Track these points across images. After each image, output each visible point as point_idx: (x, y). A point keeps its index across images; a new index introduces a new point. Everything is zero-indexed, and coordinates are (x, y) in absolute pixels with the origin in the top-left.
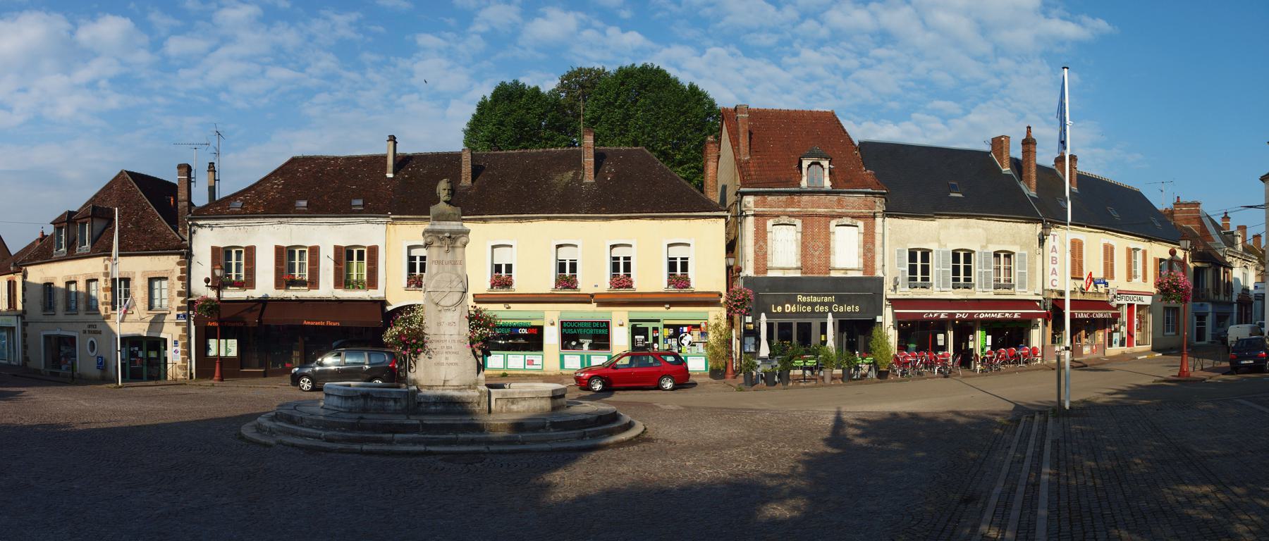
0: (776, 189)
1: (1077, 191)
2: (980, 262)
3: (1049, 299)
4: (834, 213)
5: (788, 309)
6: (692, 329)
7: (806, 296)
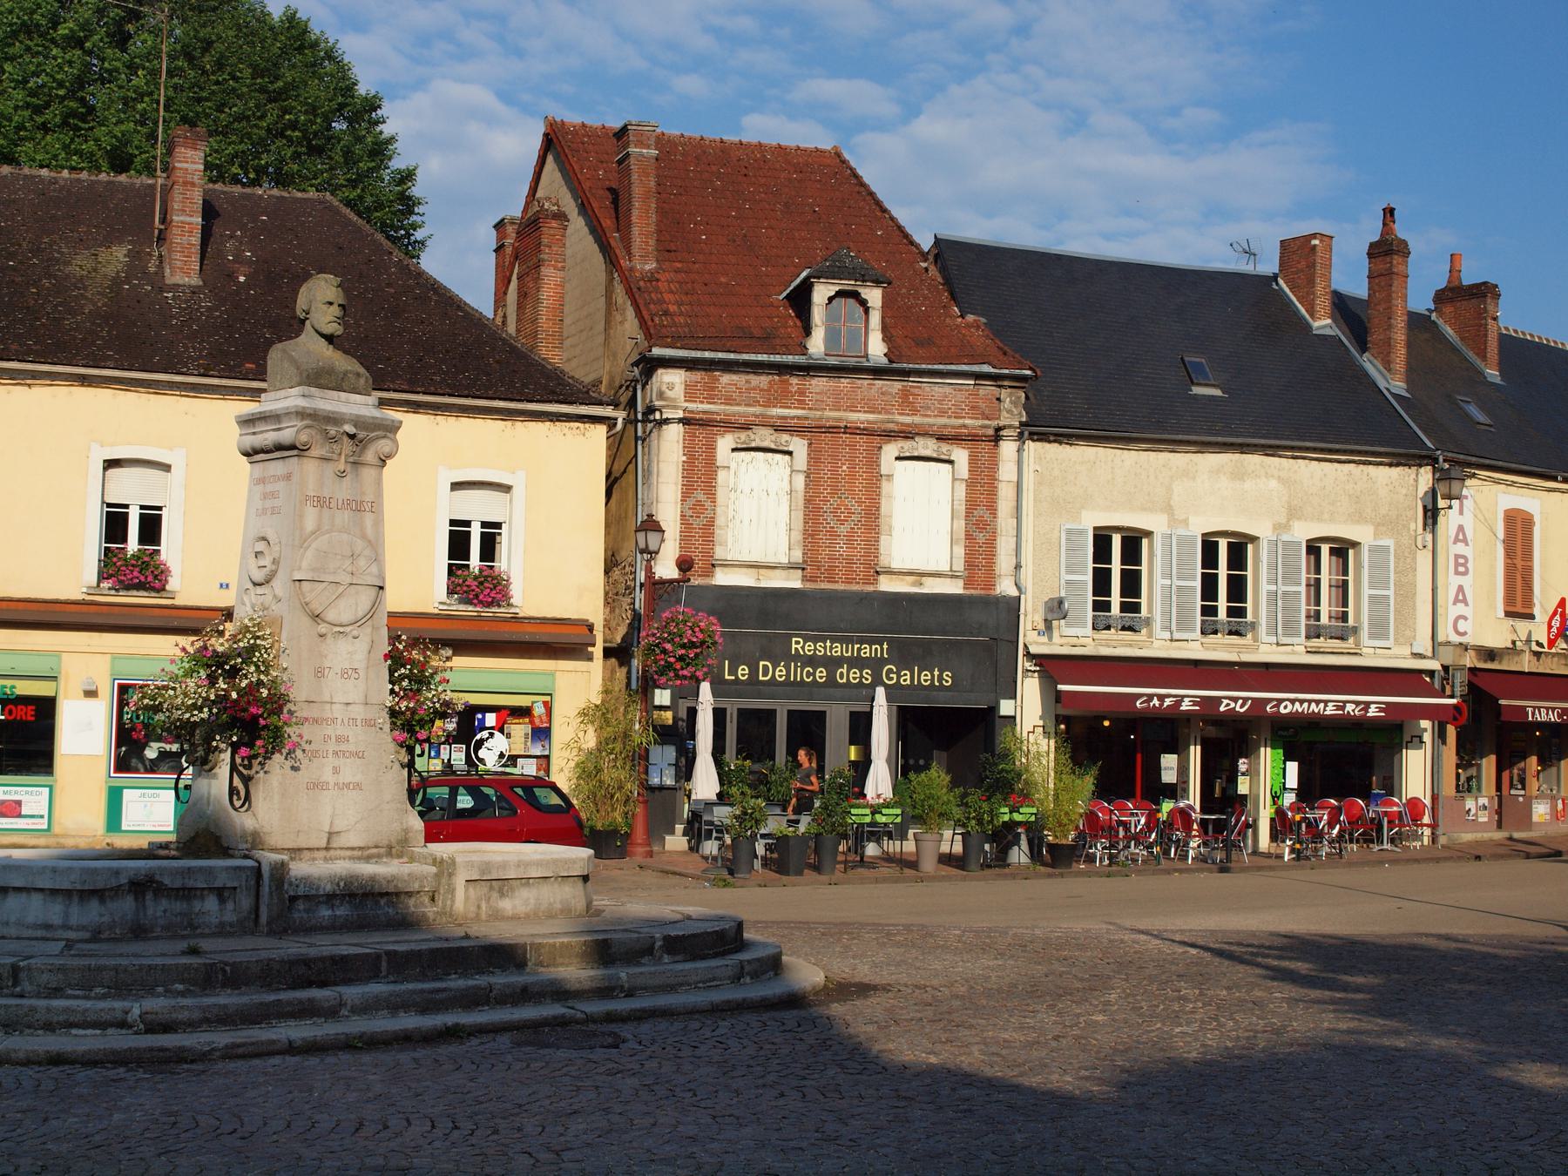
0: (745, 357)
1: (1498, 380)
2: (1273, 567)
3: (1462, 668)
4: (891, 426)
5: (765, 674)
6: (510, 720)
7: (815, 640)
